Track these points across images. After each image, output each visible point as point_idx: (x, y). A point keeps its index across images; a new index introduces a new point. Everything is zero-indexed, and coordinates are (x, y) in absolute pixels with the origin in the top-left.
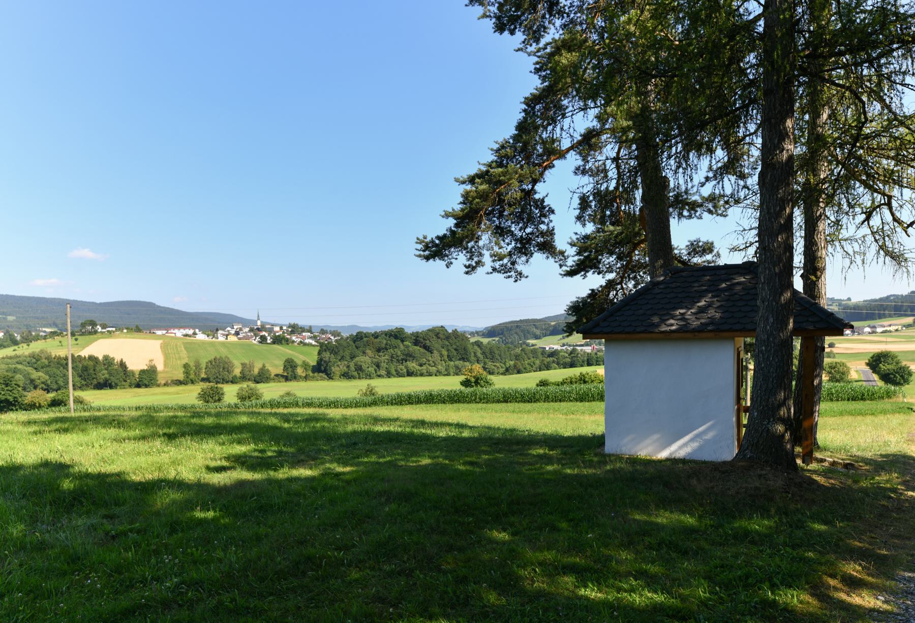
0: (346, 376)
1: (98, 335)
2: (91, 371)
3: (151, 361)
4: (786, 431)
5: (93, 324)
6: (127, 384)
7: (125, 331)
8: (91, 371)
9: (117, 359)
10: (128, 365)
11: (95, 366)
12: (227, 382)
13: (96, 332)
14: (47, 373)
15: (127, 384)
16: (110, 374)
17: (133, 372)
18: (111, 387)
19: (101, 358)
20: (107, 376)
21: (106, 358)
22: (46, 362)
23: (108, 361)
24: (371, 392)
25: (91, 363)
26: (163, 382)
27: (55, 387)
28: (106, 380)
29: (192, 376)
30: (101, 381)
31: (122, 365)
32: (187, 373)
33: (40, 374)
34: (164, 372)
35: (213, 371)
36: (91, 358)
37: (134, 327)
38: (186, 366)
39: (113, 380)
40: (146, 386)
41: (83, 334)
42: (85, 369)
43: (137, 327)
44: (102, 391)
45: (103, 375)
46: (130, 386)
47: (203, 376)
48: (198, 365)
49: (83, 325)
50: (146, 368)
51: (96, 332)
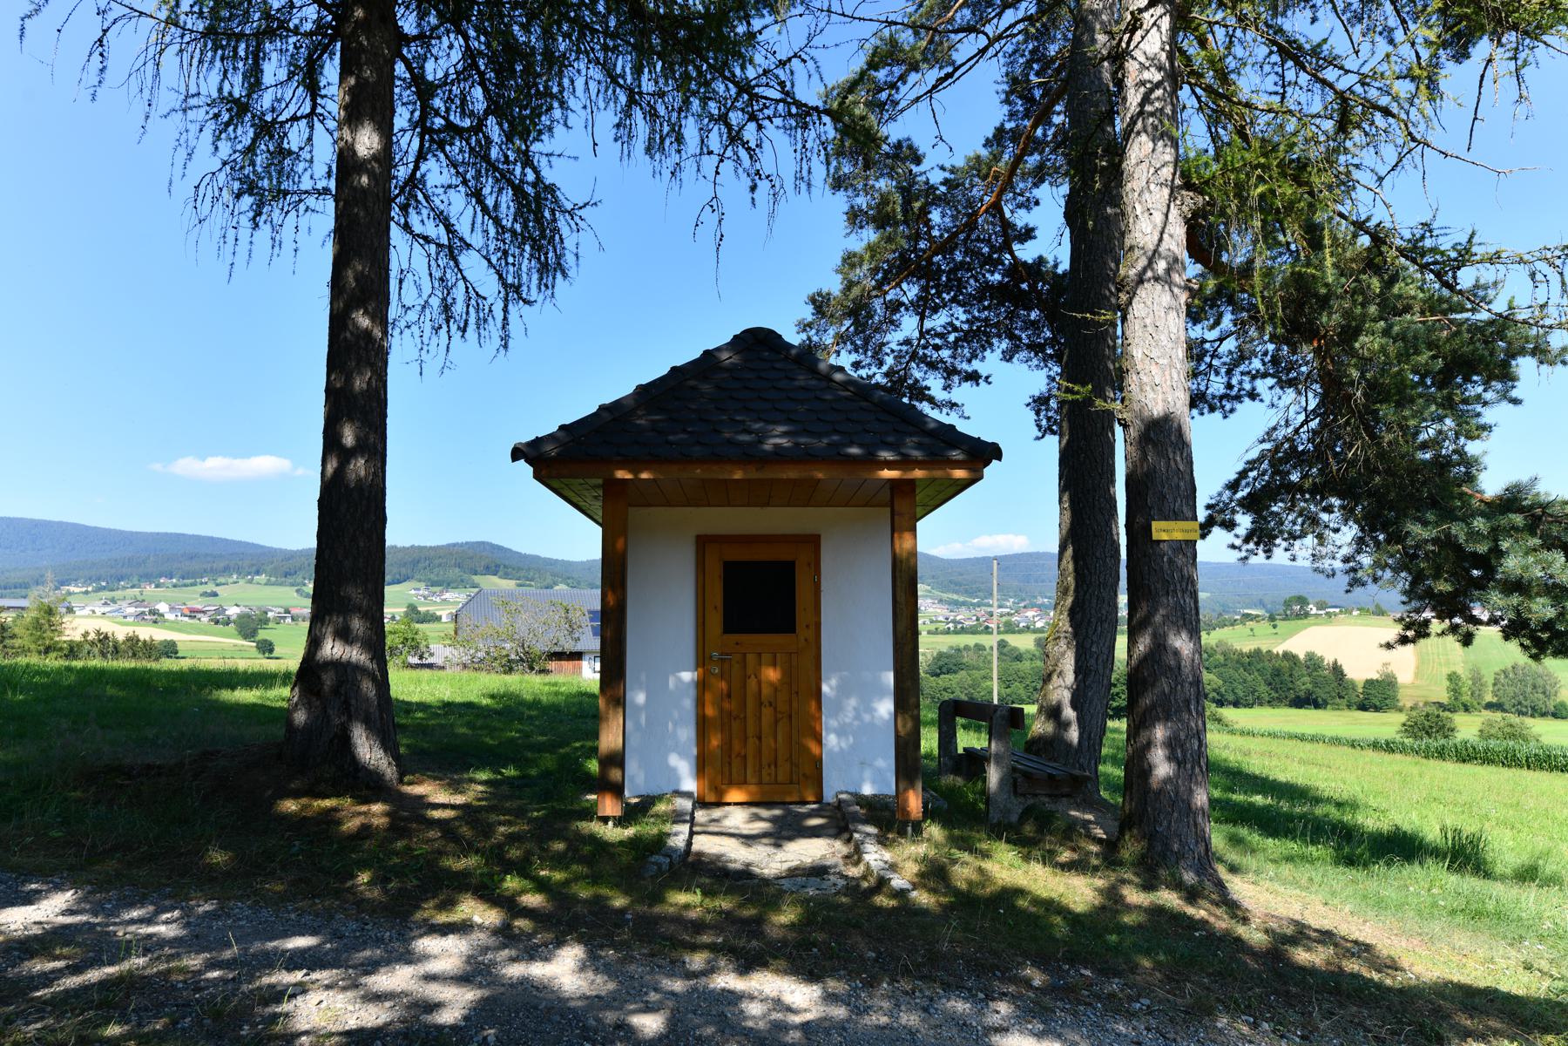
0: (1196, 352)
1: (1311, 620)
2: (1286, 677)
3: (1385, 665)
4: (1199, 649)
5: (1302, 601)
6: (1344, 702)
7: (1355, 613)
8: (1286, 677)
9: (1329, 659)
10: (1346, 670)
11: (1291, 669)
12: (1543, 715)
13: (1307, 615)
14: (1220, 676)
15: (1344, 702)
16: (1316, 684)
17: (1353, 684)
18: (1317, 706)
19: (1302, 657)
20: (1309, 686)
21: (1310, 656)
22: (1222, 658)
23: (1313, 663)
24: (1514, 734)
25: (1286, 664)
26: (1409, 704)
27: (1231, 698)
28: (1309, 693)
29: (1466, 698)
30: (1302, 694)
31: (1337, 670)
32: (1455, 691)
33: (1211, 676)
34: (1413, 686)
35: (1511, 690)
36: (1288, 656)
37: (1372, 608)
38: (1453, 677)
39: (1321, 694)
40: (1377, 709)
41: (1286, 618)
42: (1277, 673)
43: (1377, 606)
44: (1302, 711)
45: (1304, 684)
46: (1349, 707)
47: (1489, 698)
48: (1477, 679)
49: (1288, 604)
50: (1375, 676)
51: (1307, 615)
